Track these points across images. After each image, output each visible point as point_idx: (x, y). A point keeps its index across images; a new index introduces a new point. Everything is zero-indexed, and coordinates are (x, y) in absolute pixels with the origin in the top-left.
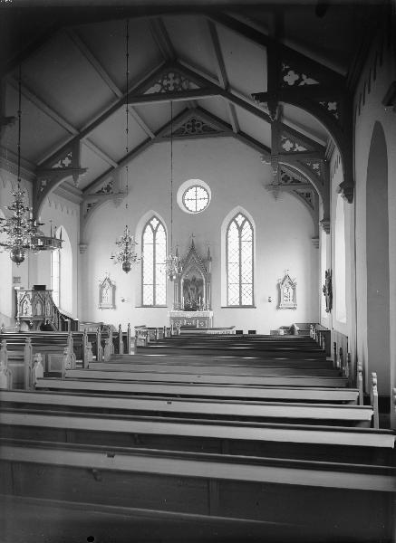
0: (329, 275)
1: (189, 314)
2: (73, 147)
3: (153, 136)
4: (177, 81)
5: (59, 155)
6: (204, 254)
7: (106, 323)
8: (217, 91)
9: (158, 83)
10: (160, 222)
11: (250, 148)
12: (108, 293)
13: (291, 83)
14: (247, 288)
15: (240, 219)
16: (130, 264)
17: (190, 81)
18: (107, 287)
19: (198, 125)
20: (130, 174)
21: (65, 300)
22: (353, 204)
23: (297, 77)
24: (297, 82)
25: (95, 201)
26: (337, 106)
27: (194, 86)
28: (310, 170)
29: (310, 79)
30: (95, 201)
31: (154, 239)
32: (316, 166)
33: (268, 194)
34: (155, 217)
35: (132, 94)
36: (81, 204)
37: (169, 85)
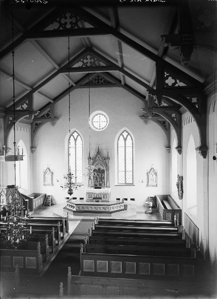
0: (181, 179)
1: (97, 191)
2: (29, 97)
3: (74, 85)
4: (74, 20)
5: (21, 101)
6: (105, 154)
7: (48, 194)
8: (116, 68)
9: (80, 61)
10: (79, 135)
11: (130, 93)
12: (48, 176)
13: (170, 84)
14: (129, 175)
15: (125, 134)
16: (72, 190)
17: (100, 61)
18: (48, 173)
19: (101, 79)
20: (61, 105)
21: (25, 189)
22: (206, 160)
23: (173, 81)
24: (174, 84)
25: (40, 122)
26: (197, 100)
27: (88, 25)
28: (169, 117)
29: (181, 83)
30: (40, 122)
31: (76, 145)
32: (173, 115)
33: (141, 121)
34: (75, 131)
35: (65, 67)
36: (32, 124)
37: (66, 23)
